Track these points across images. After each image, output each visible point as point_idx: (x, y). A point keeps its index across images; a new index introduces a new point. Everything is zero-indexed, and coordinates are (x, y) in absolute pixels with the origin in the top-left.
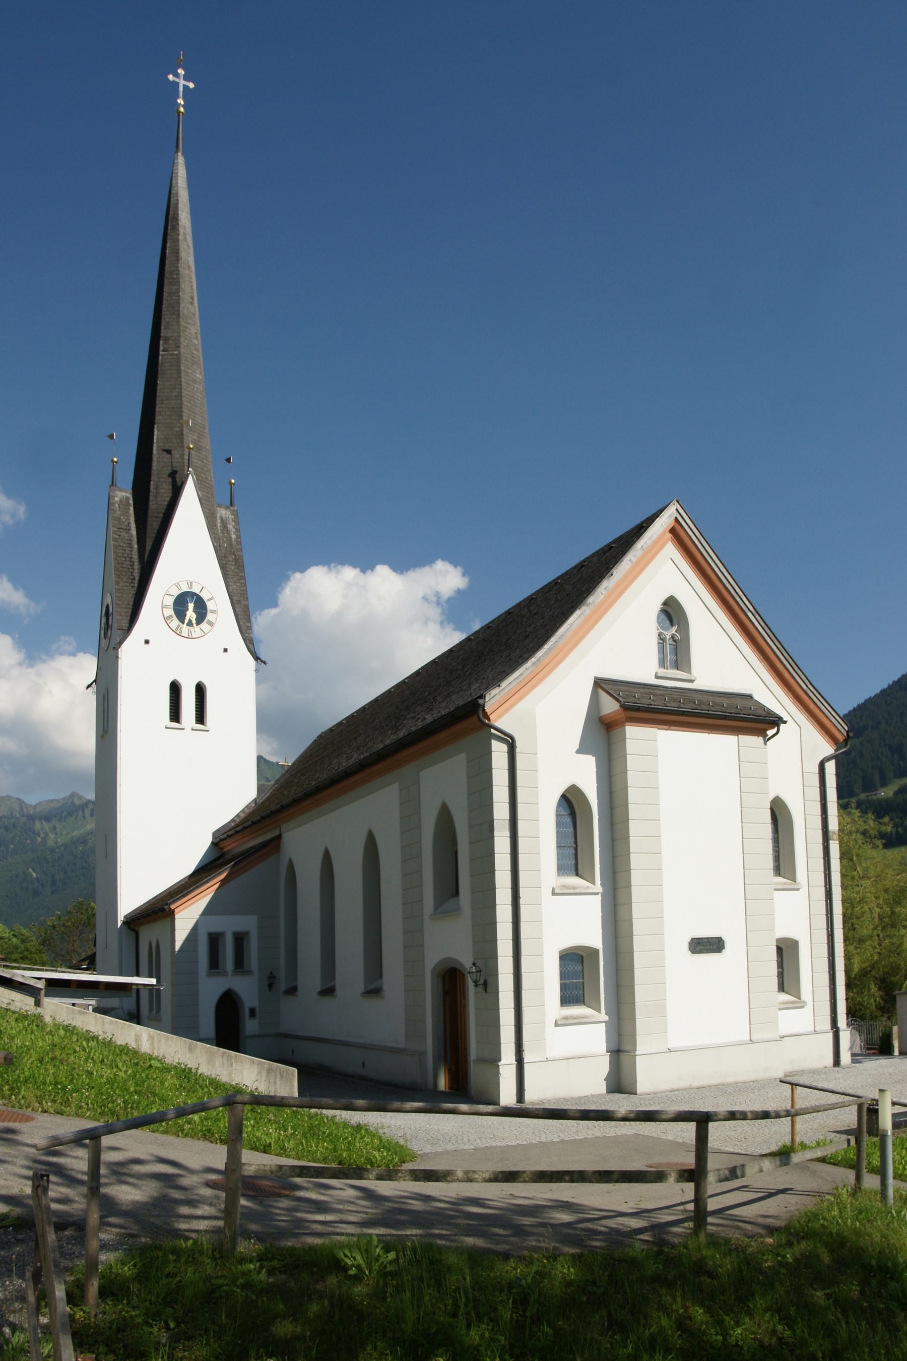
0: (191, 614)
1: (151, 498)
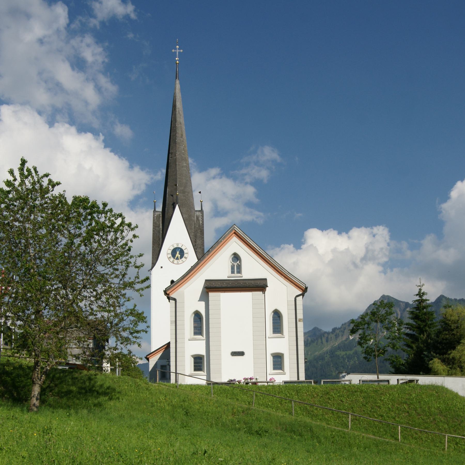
0: (178, 255)
1: (166, 214)
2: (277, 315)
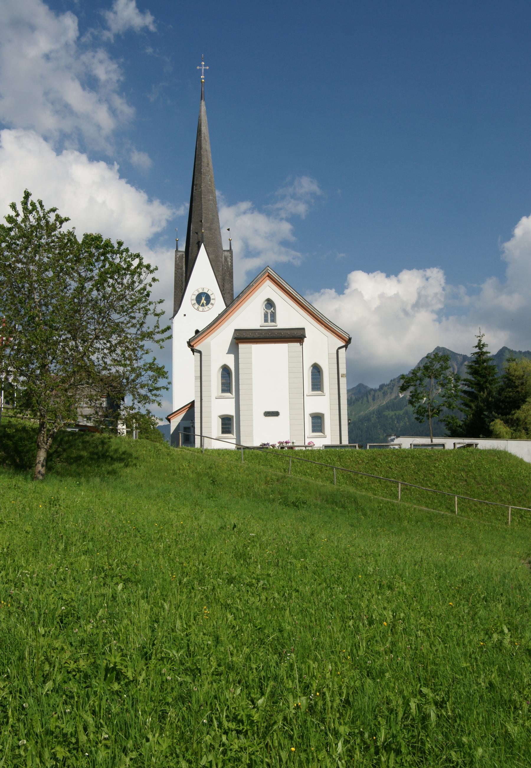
0: (203, 301)
2: (317, 370)
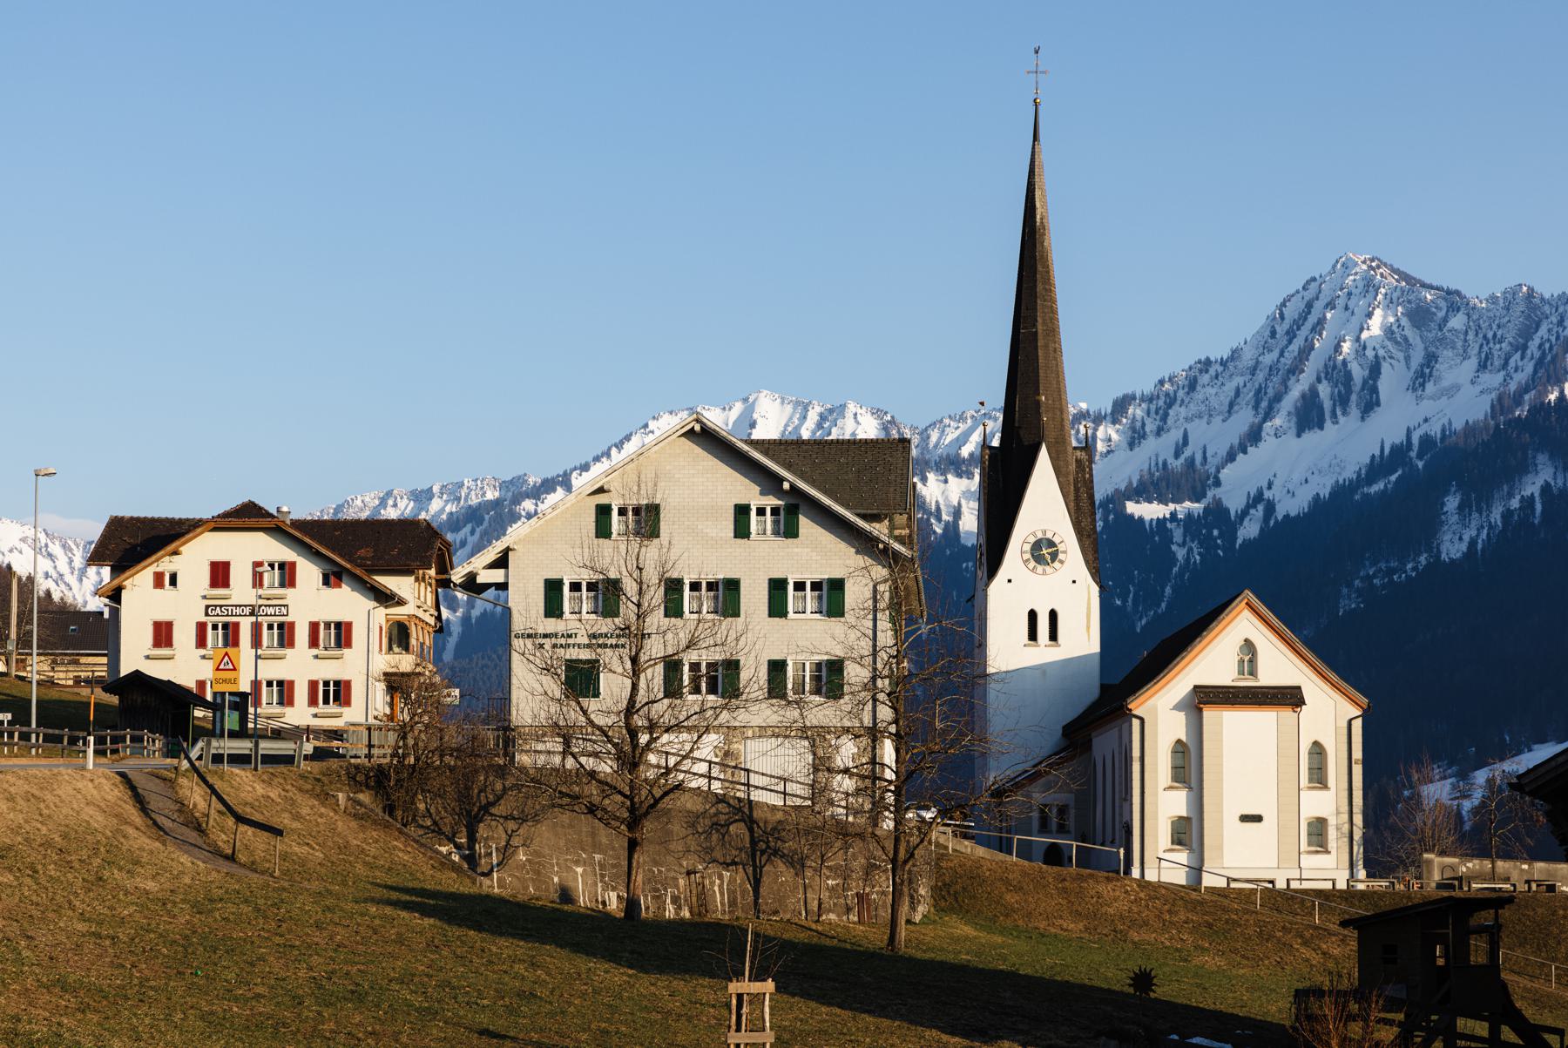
2: (1318, 750)
